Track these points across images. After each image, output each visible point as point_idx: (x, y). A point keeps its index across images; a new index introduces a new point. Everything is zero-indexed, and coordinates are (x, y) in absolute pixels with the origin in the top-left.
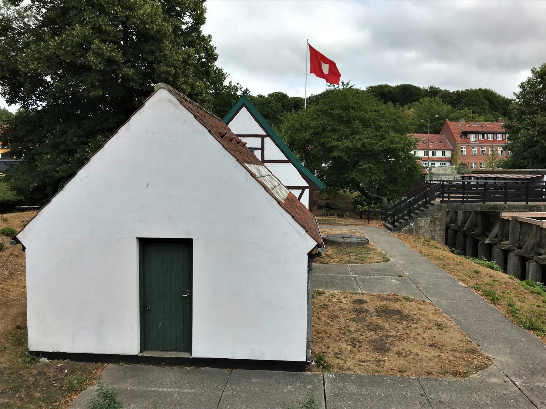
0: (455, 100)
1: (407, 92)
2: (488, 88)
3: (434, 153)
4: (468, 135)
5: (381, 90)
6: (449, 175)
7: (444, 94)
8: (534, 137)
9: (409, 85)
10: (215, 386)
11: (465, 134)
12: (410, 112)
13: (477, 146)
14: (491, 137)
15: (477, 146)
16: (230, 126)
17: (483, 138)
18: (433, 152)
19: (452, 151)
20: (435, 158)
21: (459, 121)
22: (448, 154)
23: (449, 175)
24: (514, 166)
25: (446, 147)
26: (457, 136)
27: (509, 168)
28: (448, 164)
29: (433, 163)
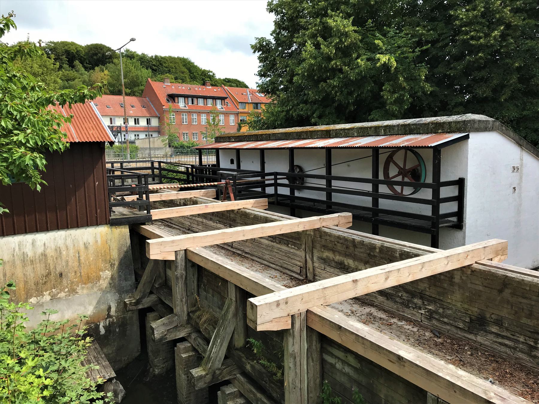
0: (155, 65)
1: (100, 53)
2: (186, 57)
3: (136, 121)
4: (176, 99)
5: (66, 48)
6: (158, 149)
7: (142, 58)
8: (329, 59)
9: (101, 44)
10: (196, 89)
11: (172, 97)
12: (102, 75)
13: (187, 112)
14: (201, 102)
15: (187, 112)
16: (430, 235)
17: (193, 103)
18: (135, 119)
19: (159, 118)
20: (138, 128)
21: (164, 82)
22: (155, 122)
23: (158, 149)
24: (289, 122)
25: (150, 113)
26: (163, 99)
27: (268, 128)
28: (155, 135)
29: (137, 134)
